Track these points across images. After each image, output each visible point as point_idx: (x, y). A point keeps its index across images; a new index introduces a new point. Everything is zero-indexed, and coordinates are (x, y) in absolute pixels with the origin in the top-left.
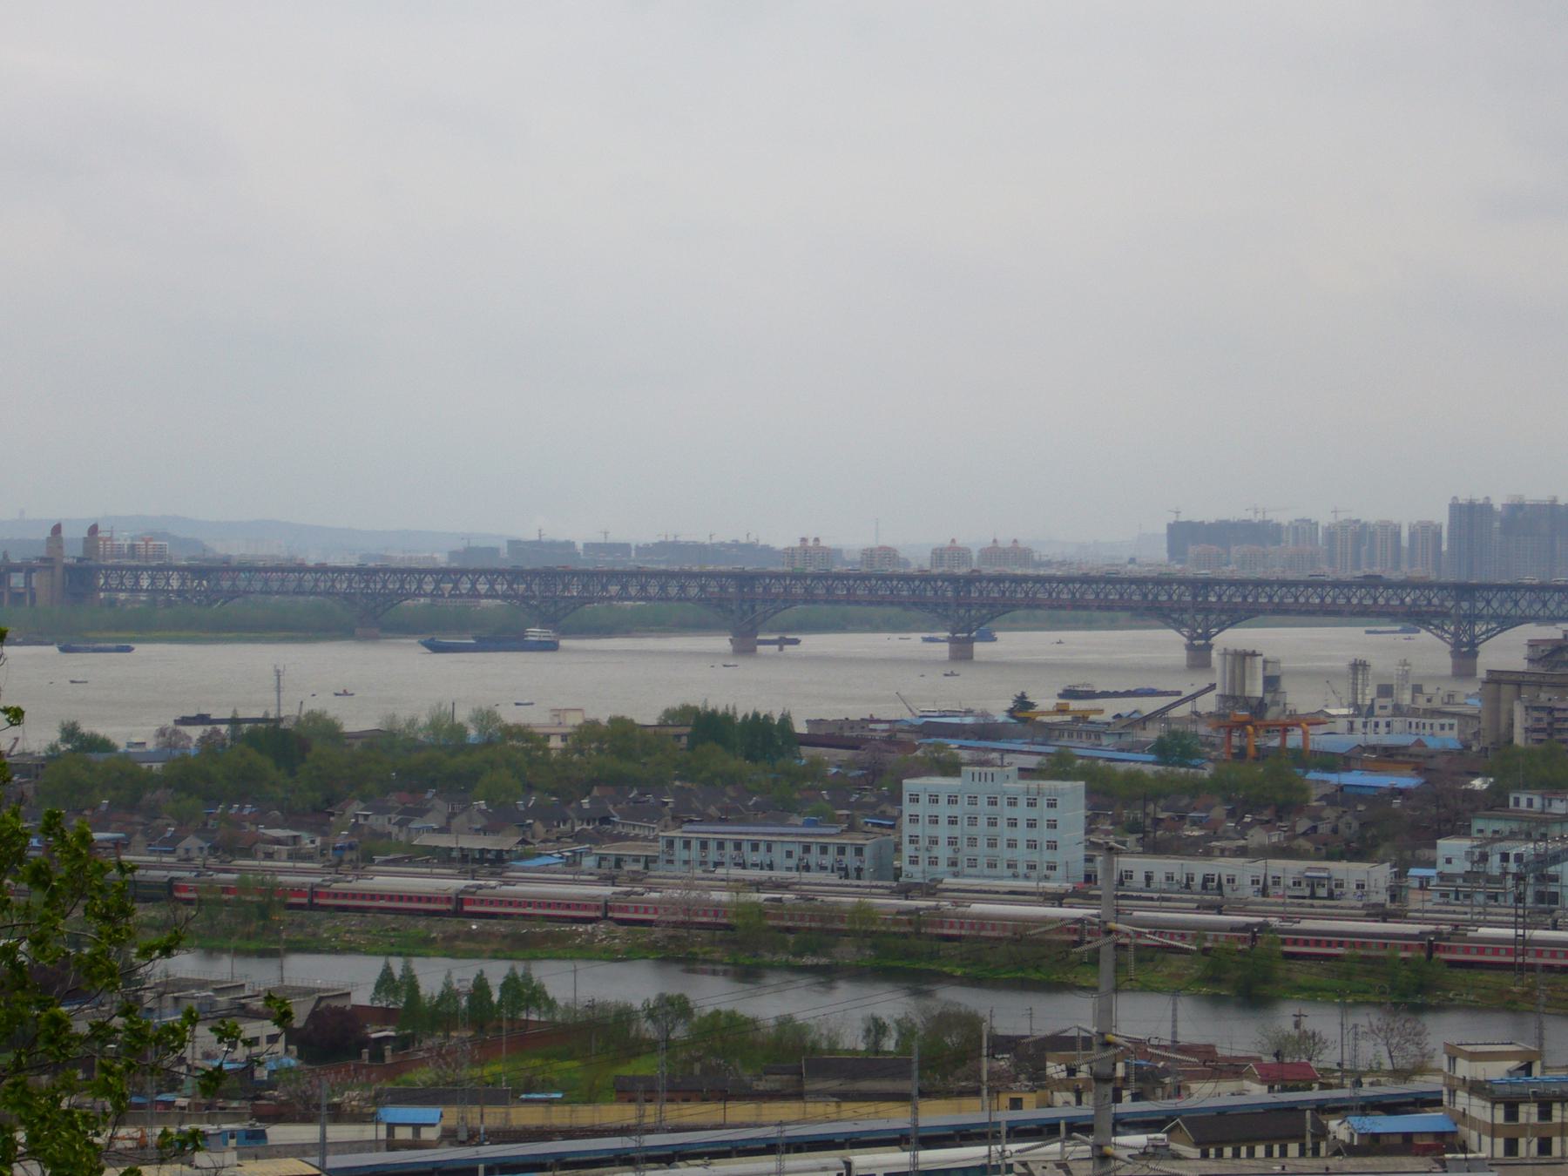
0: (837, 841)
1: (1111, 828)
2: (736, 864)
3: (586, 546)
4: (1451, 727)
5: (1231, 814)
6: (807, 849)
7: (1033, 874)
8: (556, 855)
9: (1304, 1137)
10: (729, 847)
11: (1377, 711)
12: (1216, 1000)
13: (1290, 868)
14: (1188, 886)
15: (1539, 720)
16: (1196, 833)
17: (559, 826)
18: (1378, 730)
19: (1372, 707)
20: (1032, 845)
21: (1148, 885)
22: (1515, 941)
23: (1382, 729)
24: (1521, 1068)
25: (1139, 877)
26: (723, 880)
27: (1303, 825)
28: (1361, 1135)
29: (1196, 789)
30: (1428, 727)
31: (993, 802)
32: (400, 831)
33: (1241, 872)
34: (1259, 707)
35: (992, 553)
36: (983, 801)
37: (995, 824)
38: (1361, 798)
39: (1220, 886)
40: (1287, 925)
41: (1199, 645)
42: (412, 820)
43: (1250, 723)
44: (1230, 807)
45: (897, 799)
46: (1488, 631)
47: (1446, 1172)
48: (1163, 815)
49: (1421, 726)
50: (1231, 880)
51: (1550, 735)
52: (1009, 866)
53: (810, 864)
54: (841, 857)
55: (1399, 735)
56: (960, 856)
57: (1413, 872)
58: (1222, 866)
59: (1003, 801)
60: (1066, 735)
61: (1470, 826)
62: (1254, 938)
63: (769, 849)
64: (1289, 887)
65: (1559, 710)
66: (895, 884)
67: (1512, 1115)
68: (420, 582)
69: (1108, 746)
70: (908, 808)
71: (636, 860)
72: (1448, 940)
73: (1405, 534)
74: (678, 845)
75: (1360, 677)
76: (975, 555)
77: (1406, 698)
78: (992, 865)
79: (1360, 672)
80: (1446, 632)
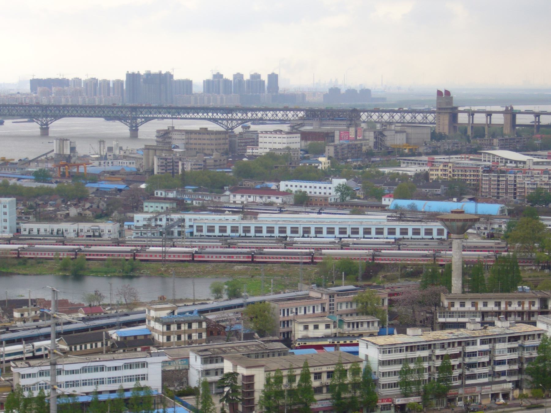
4: (133, 163)
5: (63, 201)
9: (102, 340)
11: (108, 157)
12: (65, 278)
13: (85, 227)
14: (52, 233)
15: (162, 162)
19: (106, 156)
21: (38, 233)
22: (163, 252)
23: (110, 164)
24: (171, 313)
28: (121, 337)
29: (50, 192)
33: (69, 228)
38: (106, 193)
39: (63, 233)
40: (87, 249)
43: (66, 165)
46: (141, 122)
47: (151, 357)
48: (40, 203)
50: (66, 231)
51: (166, 167)
55: (116, 166)
57: (126, 223)
58: (63, 226)
61: (143, 204)
62: (76, 255)
67: (169, 328)
72: (140, 252)
75: (102, 146)
77: (117, 152)
80: (128, 122)
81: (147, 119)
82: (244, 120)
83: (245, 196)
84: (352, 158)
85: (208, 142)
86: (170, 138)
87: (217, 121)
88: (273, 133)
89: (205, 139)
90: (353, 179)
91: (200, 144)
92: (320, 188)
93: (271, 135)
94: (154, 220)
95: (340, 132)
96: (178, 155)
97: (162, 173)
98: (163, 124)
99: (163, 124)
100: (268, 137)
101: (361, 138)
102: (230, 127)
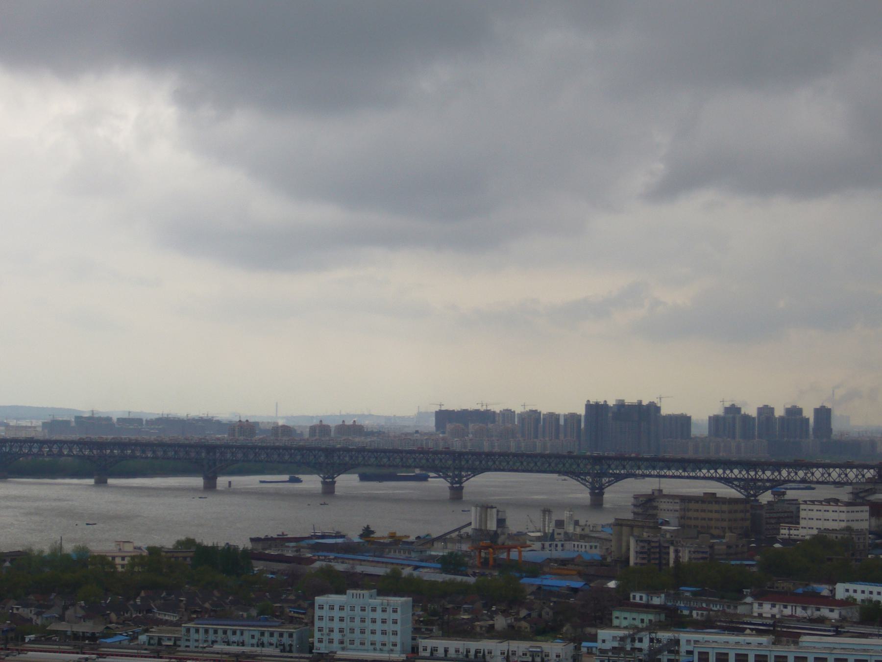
0: (279, 630)
1: (421, 613)
2: (224, 642)
3: (118, 419)
4: (596, 547)
6: (262, 634)
7: (385, 648)
8: (124, 634)
10: (220, 632)
11: (556, 536)
16: (465, 617)
17: (124, 614)
19: (553, 534)
20: (384, 633)
21: (446, 655)
23: (559, 548)
26: (218, 653)
27: (523, 613)
29: (465, 589)
30: (583, 547)
31: (363, 609)
32: (37, 618)
34: (495, 535)
36: (358, 609)
37: (364, 621)
41: (456, 487)
42: (44, 612)
43: (490, 547)
44: (484, 602)
45: (312, 605)
46: (609, 481)
49: (580, 546)
50: (490, 652)
52: (372, 644)
53: (264, 642)
54: (281, 638)
55: (570, 550)
56: (345, 638)
57: (584, 644)
59: (369, 609)
60: (392, 551)
63: (242, 634)
64: (520, 656)
65: (653, 542)
66: (311, 656)
68: (31, 447)
69: (415, 557)
70: (318, 613)
71: (169, 639)
73: (562, 422)
74: (192, 631)
75: (547, 518)
77: (570, 529)
78: (362, 644)
79: (547, 515)
80: (587, 482)
81: (619, 478)
83: (777, 606)
86: (656, 508)
87: (730, 483)
88: (824, 503)
93: (820, 507)
94: (629, 640)
96: (668, 536)
97: (642, 564)
98: (646, 486)
99: (646, 486)
100: (831, 511)
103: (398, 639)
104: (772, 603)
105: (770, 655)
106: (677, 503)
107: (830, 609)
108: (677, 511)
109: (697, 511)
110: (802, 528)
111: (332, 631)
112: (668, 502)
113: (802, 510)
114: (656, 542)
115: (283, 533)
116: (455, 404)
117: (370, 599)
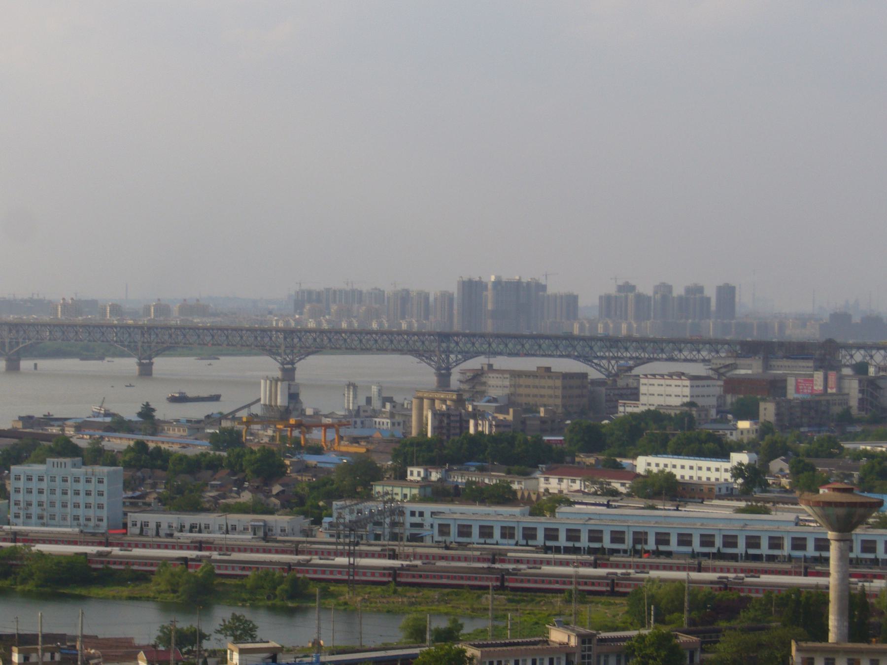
18: (356, 426)
20: (88, 506)
25: (152, 525)
31: (65, 480)
35: (188, 308)
36: (58, 480)
65: (453, 415)
73: (431, 299)
76: (175, 309)
80: (433, 361)
82: (640, 359)
83: (565, 481)
84: (809, 426)
85: (550, 392)
86: (484, 384)
87: (589, 361)
88: (666, 377)
89: (544, 387)
90: (783, 457)
91: (536, 396)
92: (709, 469)
93: (662, 382)
95: (796, 380)
100: (673, 386)
101: (834, 391)
102: (613, 372)
103: (104, 513)
104: (560, 477)
105: (518, 527)
106: (507, 378)
107: (621, 483)
108: (507, 387)
109: (529, 387)
110: (642, 404)
111: (31, 505)
112: (497, 378)
113: (643, 384)
114: (457, 415)
115: (49, 413)
116: (317, 284)
117: (73, 468)
